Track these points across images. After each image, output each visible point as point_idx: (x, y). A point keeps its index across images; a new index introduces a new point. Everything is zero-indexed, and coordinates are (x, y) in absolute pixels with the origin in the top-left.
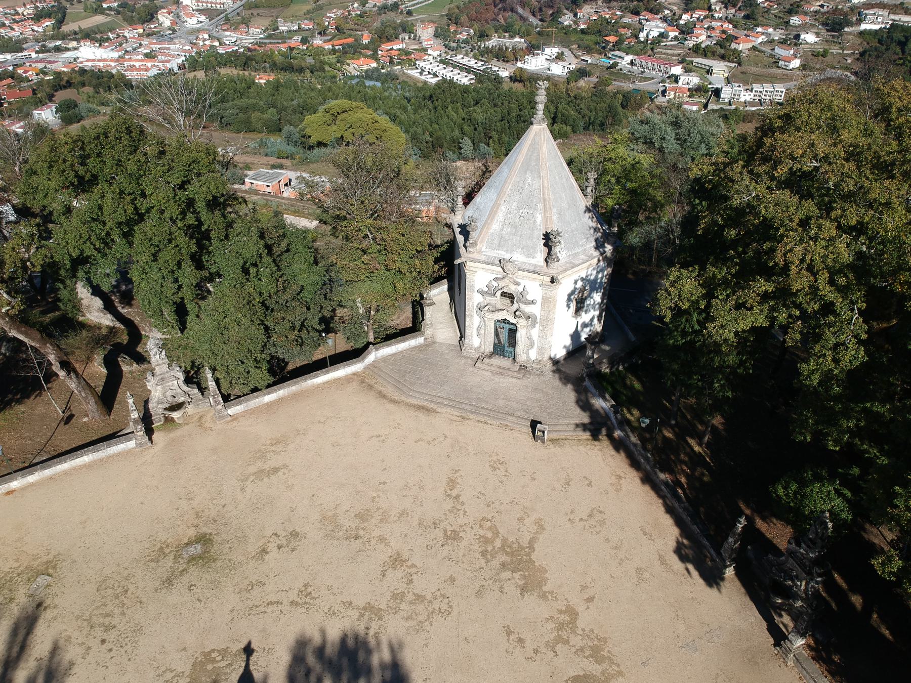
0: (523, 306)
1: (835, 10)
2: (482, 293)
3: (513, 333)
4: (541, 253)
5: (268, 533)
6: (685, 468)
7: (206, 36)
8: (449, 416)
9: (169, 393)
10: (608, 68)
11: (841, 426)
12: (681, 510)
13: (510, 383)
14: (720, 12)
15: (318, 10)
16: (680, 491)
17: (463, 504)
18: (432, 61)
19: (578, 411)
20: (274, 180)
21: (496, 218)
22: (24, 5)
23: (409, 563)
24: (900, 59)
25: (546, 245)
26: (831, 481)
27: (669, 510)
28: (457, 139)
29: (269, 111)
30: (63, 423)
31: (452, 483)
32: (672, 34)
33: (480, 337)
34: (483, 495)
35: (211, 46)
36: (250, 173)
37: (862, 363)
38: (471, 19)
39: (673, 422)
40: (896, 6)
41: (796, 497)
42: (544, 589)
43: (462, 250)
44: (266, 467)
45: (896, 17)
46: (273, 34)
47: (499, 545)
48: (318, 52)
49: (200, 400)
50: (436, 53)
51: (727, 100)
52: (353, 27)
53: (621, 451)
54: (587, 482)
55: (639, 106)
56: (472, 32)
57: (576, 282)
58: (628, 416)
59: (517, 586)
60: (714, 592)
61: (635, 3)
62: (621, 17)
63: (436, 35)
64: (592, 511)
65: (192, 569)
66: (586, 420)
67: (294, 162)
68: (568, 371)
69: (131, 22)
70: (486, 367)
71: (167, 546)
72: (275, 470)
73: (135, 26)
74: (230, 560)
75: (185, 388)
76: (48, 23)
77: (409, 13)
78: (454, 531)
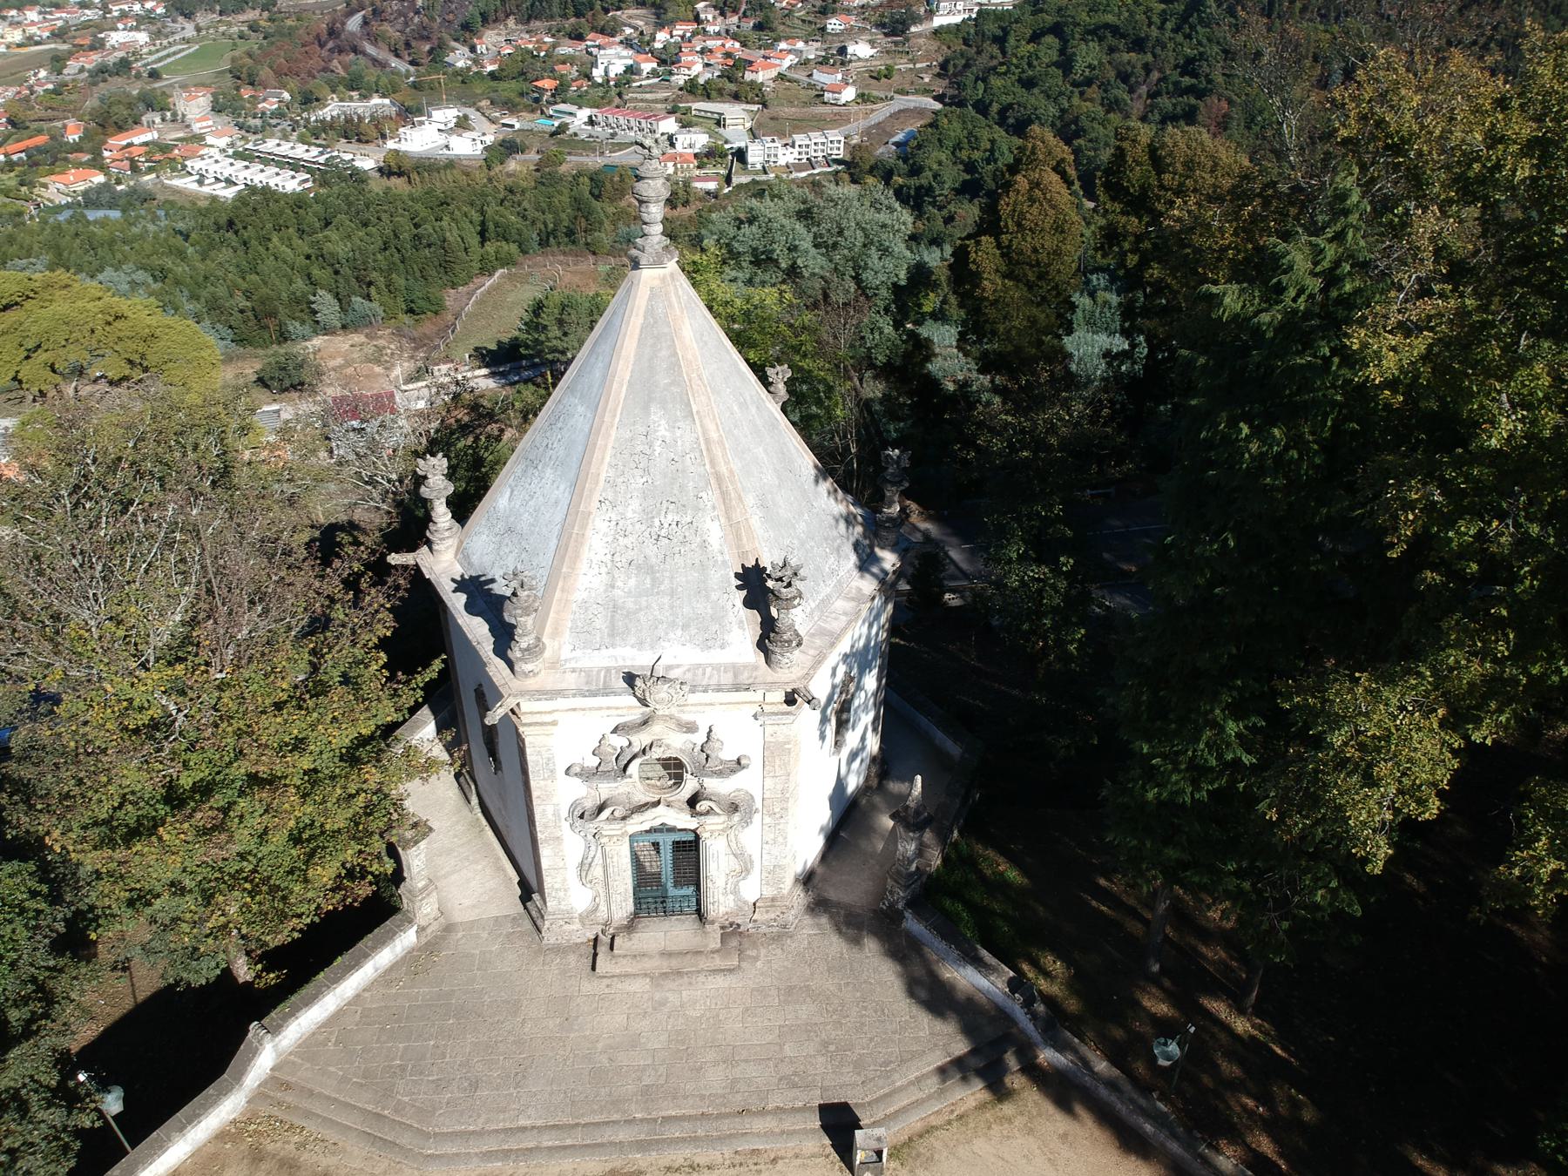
0: (713, 785)
2: (589, 775)
3: (688, 850)
4: (745, 626)
10: (553, 135)
13: (714, 996)
18: (218, 156)
21: (585, 554)
24: (1002, 64)
32: (648, 66)
33: (586, 876)
38: (279, 73)
43: (496, 668)
50: (223, 142)
51: (759, 167)
52: (43, 114)
53: (1079, 1109)
56: (286, 96)
61: (573, 20)
62: (554, 46)
63: (217, 109)
66: (961, 1047)
70: (626, 966)
77: (154, 75)
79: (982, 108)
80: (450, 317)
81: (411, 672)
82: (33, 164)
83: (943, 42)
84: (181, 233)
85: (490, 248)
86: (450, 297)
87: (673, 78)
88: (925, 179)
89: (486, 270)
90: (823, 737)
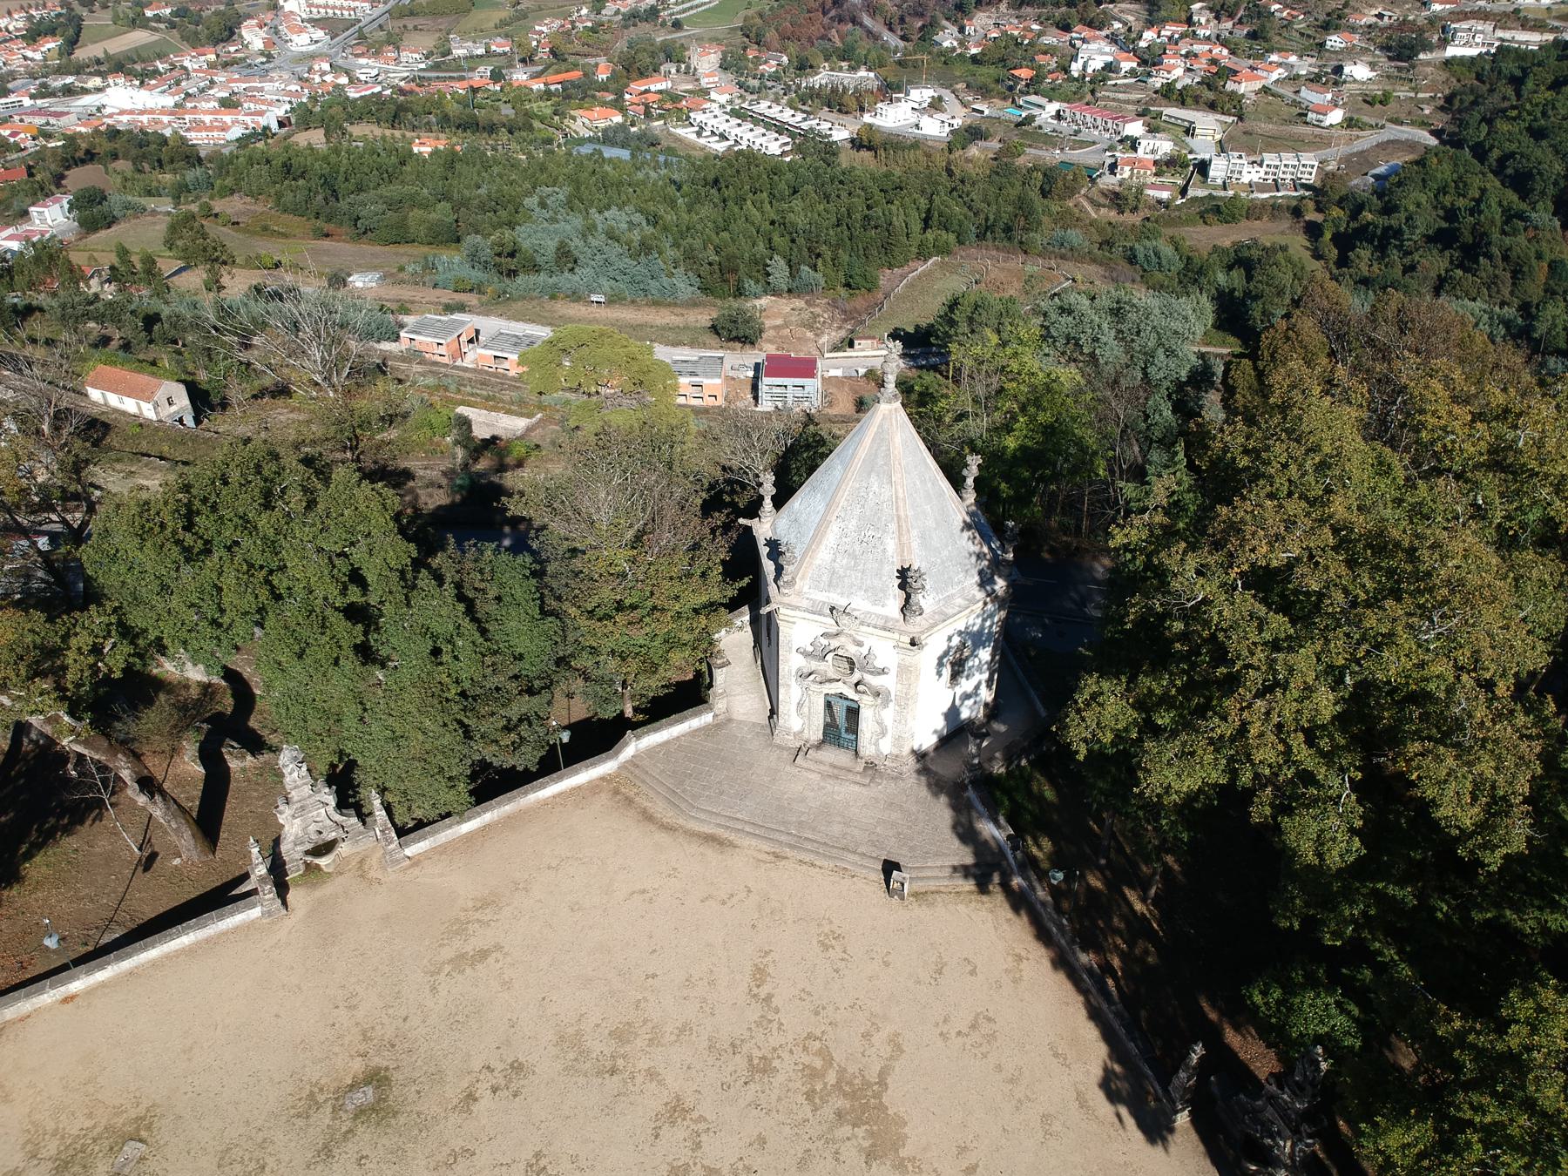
0: (868, 678)
1: (1403, 24)
2: (806, 654)
3: (853, 713)
4: (895, 598)
5: (477, 1064)
6: (1119, 941)
7: (326, 67)
8: (756, 854)
9: (313, 828)
10: (1018, 125)
11: (1341, 914)
12: (1111, 1016)
13: (848, 792)
14: (1206, 24)
15: (520, 19)
16: (1110, 982)
17: (777, 1011)
18: (717, 112)
19: (956, 843)
20: (450, 333)
21: (825, 542)
22: (10, 13)
23: (695, 1115)
24: (1514, 107)
25: (902, 586)
26: (1330, 991)
27: (1094, 1015)
28: (763, 258)
29: (440, 206)
30: (140, 869)
31: (760, 975)
32: (1127, 65)
33: (802, 715)
34: (809, 994)
35: (337, 86)
36: (409, 320)
37: (1359, 859)
38: (785, 37)
39: (1103, 862)
40: (1505, 14)
41: (1278, 1010)
42: (903, 1153)
43: (772, 589)
44: (469, 948)
45: (1507, 35)
46: (442, 62)
47: (833, 1081)
48: (520, 97)
49: (361, 833)
50: (723, 99)
51: (1219, 182)
52: (579, 48)
53: (1023, 912)
54: (970, 968)
55: (1071, 191)
56: (785, 59)
57: (950, 639)
58: (1035, 850)
59: (861, 1149)
60: (1157, 1152)
61: (1064, 9)
63: (724, 66)
64: (976, 1018)
65: (361, 1129)
66: (969, 860)
67: (484, 298)
68: (941, 771)
69: (194, 41)
71: (321, 1090)
72: (483, 955)
73: (201, 50)
74: (419, 1114)
75: (338, 817)
76: (51, 44)
77: (677, 25)
78: (763, 1058)
79: (1480, 152)
80: (881, 296)
81: (734, 580)
82: (567, 96)
83: (1453, 74)
84: (675, 182)
85: (930, 235)
86: (885, 277)
87: (1150, 80)
88: (1396, 220)
89: (923, 256)
90: (939, 674)
